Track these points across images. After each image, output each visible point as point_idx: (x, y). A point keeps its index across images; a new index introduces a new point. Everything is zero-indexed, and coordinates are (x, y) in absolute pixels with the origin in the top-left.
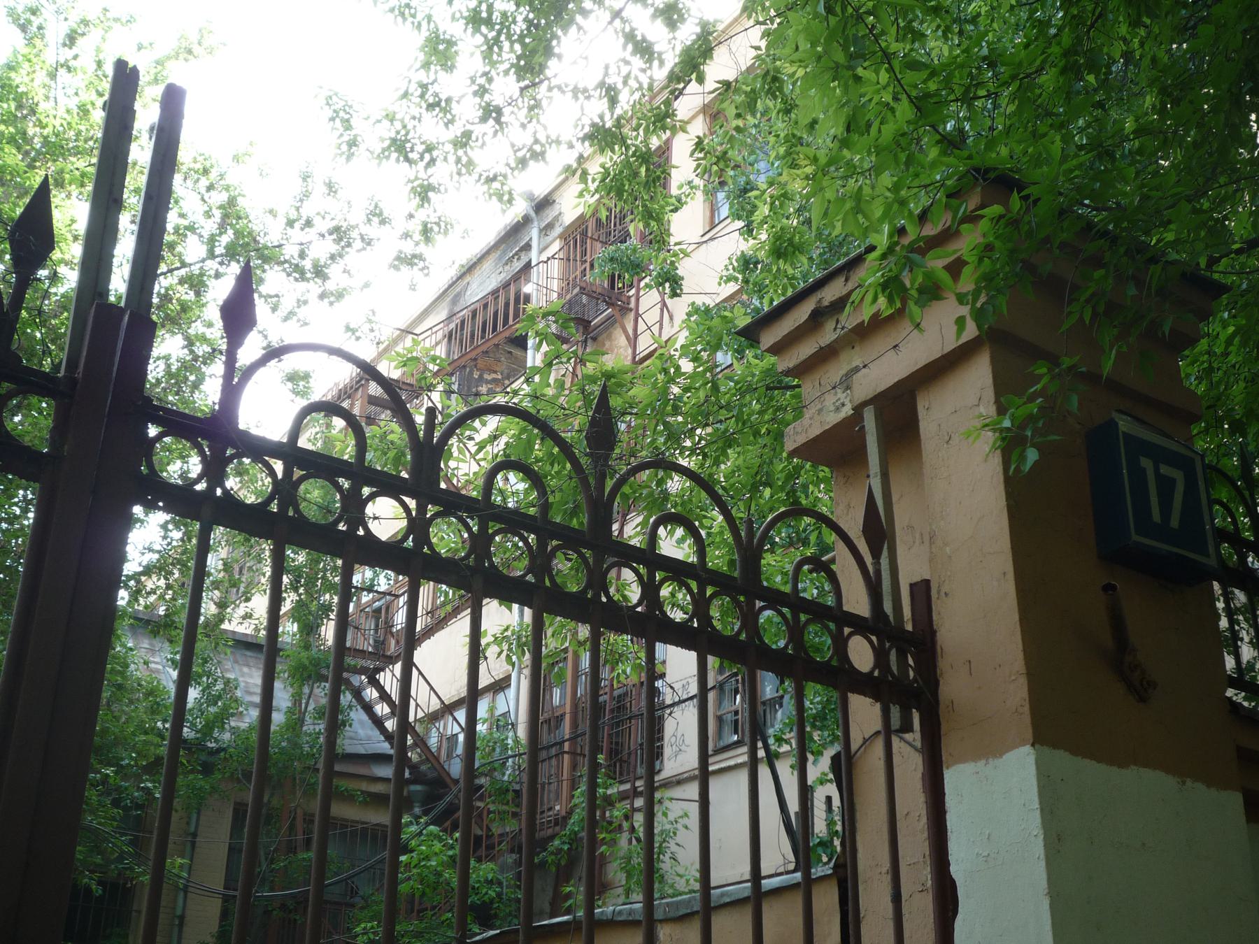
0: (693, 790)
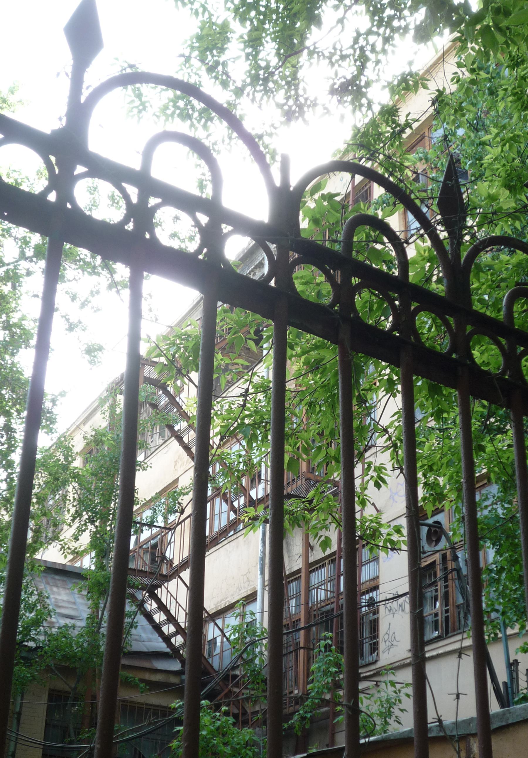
0: (407, 676)
